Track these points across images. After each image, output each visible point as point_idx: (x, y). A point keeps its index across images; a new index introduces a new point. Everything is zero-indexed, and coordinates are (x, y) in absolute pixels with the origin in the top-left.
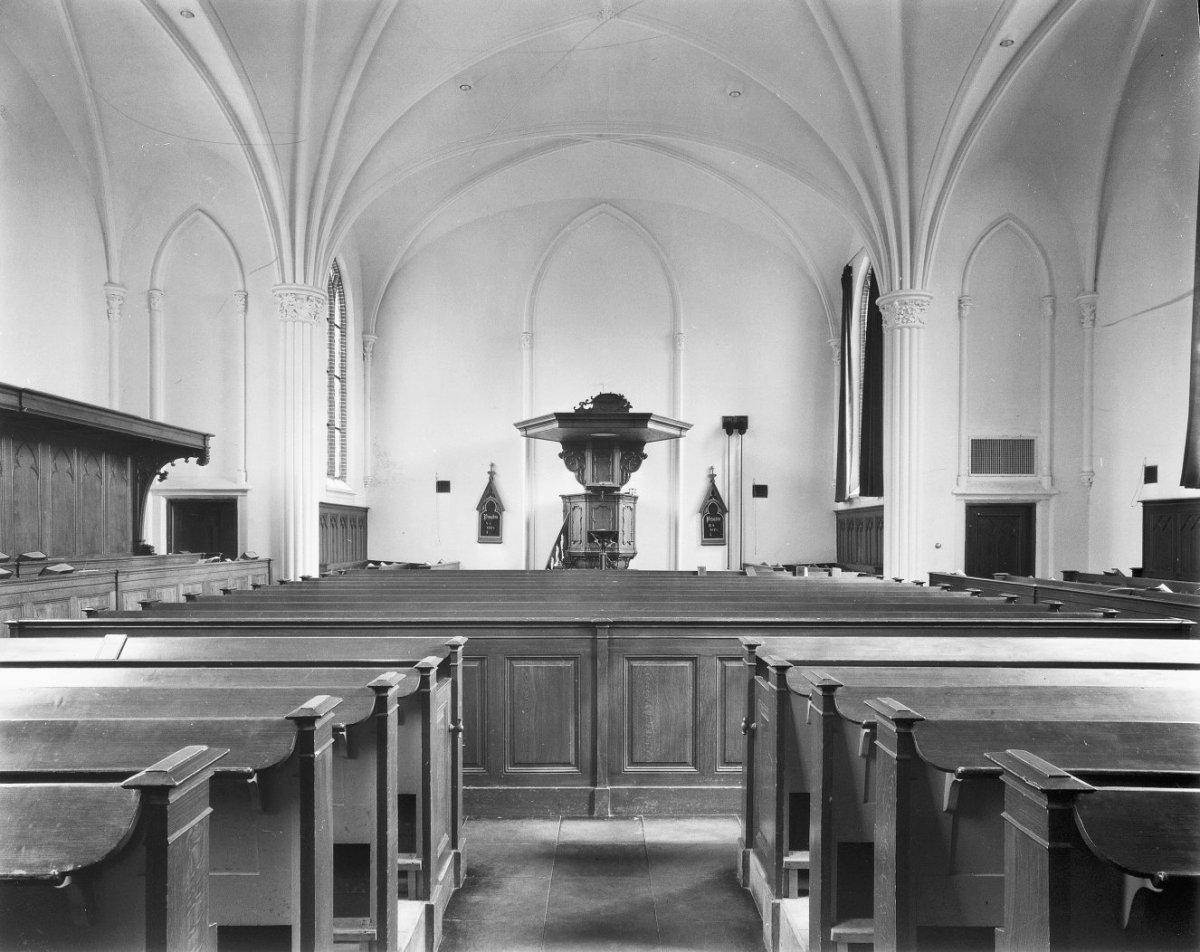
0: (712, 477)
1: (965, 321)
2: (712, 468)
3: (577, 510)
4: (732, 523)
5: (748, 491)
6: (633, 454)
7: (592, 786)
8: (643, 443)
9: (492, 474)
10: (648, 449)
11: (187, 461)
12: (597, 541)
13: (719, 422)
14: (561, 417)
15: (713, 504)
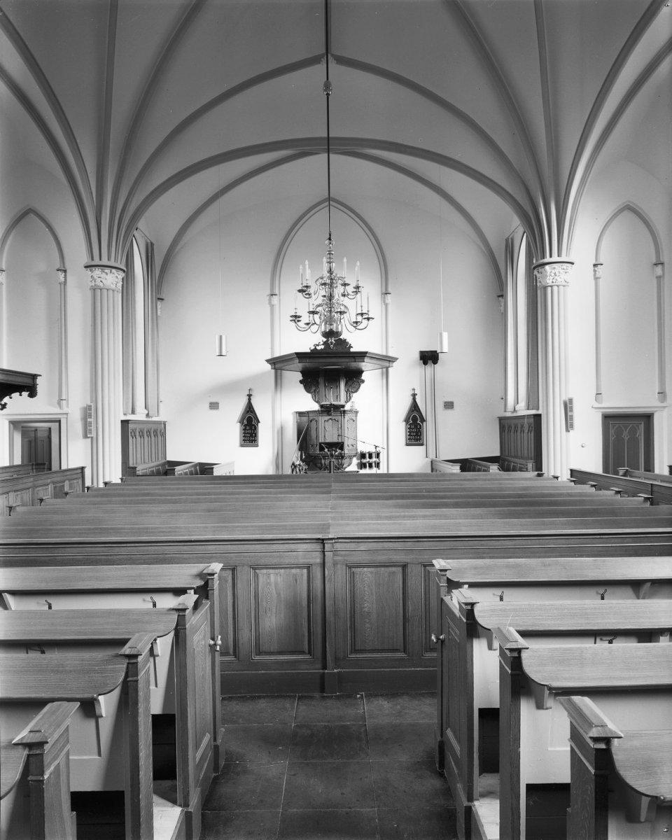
0: (414, 395)
2: (414, 389)
3: (314, 422)
5: (440, 405)
6: (353, 377)
7: (323, 669)
8: (362, 372)
9: (250, 399)
10: (364, 376)
11: (21, 395)
12: (326, 450)
13: (417, 356)
14: (301, 356)
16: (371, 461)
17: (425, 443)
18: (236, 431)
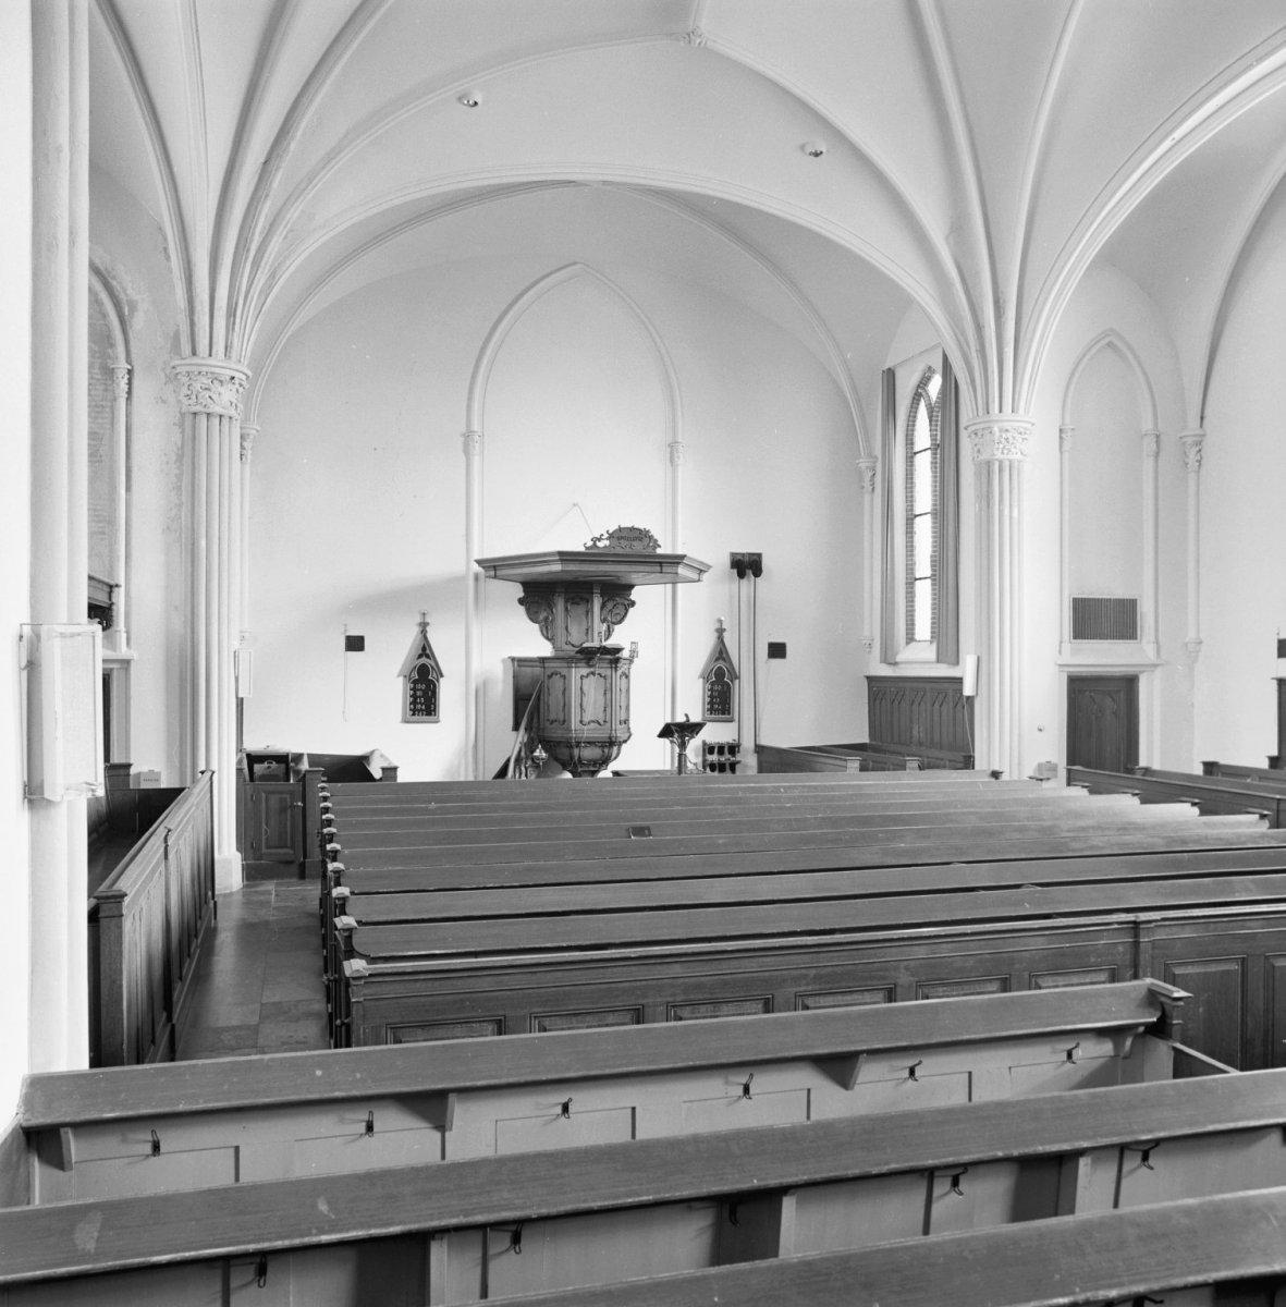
0: (720, 632)
1: (1066, 455)
3: (556, 678)
4: (743, 694)
5: (763, 651)
9: (424, 633)
10: (635, 594)
15: (720, 668)
16: (723, 759)
17: (736, 718)
18: (396, 692)
